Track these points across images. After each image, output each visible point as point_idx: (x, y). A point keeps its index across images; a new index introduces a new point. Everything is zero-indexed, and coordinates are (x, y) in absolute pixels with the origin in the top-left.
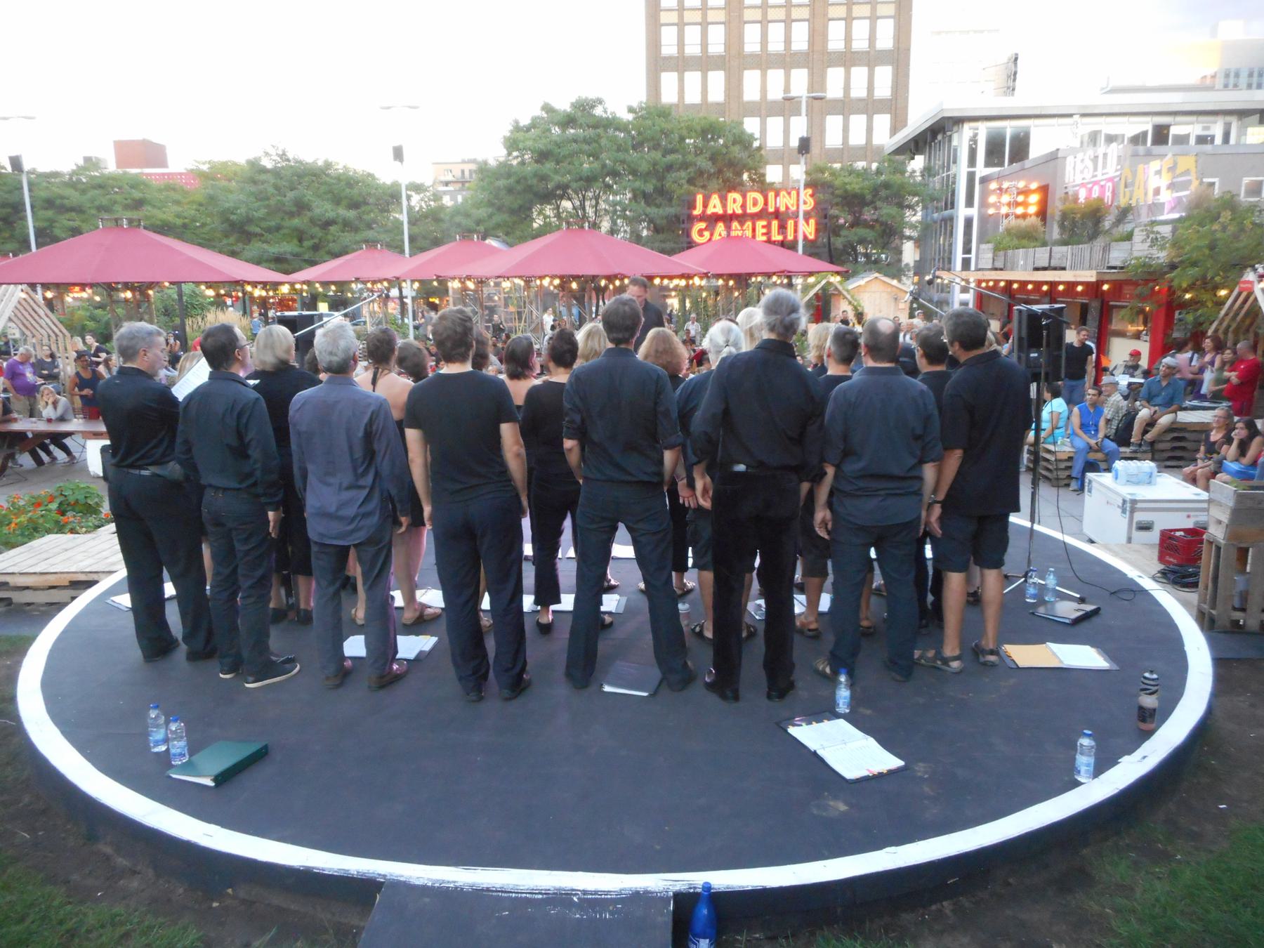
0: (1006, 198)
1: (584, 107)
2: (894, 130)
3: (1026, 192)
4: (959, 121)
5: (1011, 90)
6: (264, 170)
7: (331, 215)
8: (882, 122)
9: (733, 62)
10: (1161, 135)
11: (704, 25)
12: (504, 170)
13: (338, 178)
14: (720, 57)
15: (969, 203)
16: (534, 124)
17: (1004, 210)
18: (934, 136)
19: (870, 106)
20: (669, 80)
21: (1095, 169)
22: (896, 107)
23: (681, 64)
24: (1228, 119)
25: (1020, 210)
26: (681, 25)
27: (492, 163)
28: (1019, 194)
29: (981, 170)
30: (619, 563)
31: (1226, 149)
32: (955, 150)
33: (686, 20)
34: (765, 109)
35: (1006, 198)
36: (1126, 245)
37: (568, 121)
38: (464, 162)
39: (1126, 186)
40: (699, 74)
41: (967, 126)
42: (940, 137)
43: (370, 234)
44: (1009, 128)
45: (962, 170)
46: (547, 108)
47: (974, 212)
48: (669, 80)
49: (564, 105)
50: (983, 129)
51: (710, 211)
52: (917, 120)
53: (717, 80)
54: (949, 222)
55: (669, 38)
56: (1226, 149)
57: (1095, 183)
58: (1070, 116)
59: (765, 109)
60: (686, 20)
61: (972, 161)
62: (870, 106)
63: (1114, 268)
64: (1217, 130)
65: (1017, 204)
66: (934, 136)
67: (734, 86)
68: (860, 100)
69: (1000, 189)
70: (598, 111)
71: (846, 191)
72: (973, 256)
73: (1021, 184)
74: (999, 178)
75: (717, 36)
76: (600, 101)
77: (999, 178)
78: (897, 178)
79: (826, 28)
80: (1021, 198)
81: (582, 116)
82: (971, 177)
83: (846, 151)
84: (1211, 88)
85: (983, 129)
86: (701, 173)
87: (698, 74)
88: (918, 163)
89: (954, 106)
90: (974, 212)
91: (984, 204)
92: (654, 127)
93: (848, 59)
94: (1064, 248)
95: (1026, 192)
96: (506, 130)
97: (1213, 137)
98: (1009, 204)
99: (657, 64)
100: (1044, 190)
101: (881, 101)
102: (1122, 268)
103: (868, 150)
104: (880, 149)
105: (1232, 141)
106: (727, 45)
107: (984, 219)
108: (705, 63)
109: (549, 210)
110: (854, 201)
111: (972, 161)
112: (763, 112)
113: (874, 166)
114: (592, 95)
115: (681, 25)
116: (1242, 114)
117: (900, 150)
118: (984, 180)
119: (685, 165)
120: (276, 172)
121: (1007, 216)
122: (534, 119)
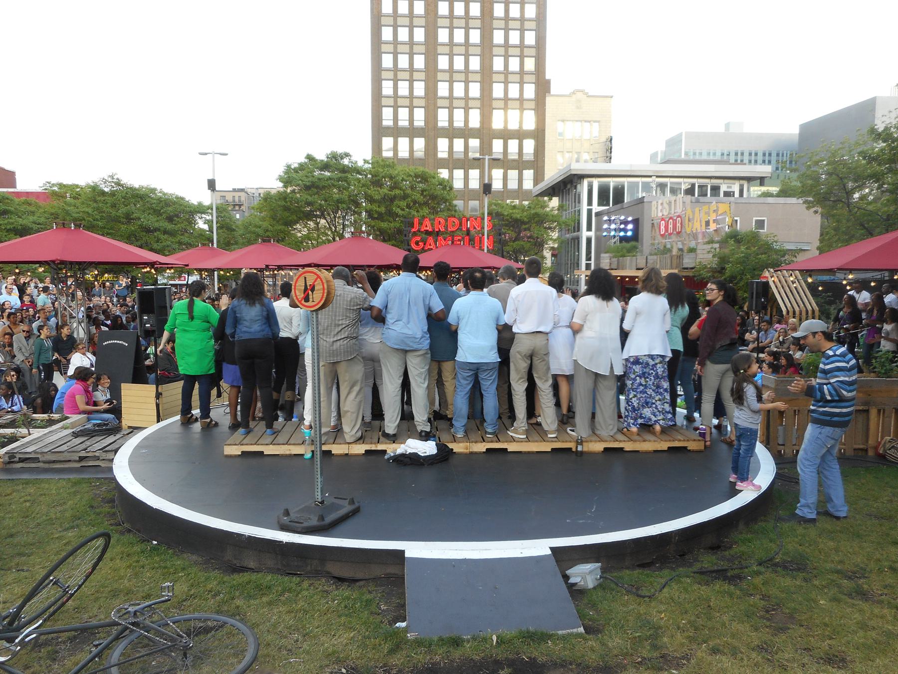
0: (613, 226)
1: (334, 156)
2: (536, 181)
3: (626, 223)
4: (581, 177)
5: (609, 159)
6: (103, 193)
7: (156, 225)
8: (528, 174)
9: (431, 132)
10: (715, 189)
11: (411, 108)
12: (282, 196)
13: (160, 200)
14: (422, 129)
15: (589, 229)
16: (302, 167)
17: (613, 233)
18: (565, 186)
19: (520, 164)
20: (387, 142)
21: (670, 209)
22: (537, 164)
23: (396, 132)
24: (742, 182)
25: (622, 234)
26: (396, 108)
27: (273, 192)
28: (621, 224)
29: (596, 208)
30: (512, 455)
31: (741, 200)
32: (579, 195)
33: (399, 104)
34: (452, 163)
35: (613, 226)
36: (692, 255)
37: (325, 166)
38: (234, 190)
39: (689, 221)
40: (392, 139)
41: (586, 182)
42: (569, 186)
43: (185, 239)
44: (612, 182)
45: (585, 207)
46: (310, 158)
47: (592, 234)
48: (387, 142)
49: (321, 156)
50: (596, 183)
51: (423, 229)
52: (553, 172)
53: (420, 143)
54: (577, 240)
55: (387, 114)
56: (741, 200)
57: (671, 218)
58: (650, 176)
59: (452, 163)
60: (399, 104)
61: (590, 203)
62: (520, 164)
63: (687, 269)
64: (736, 188)
65: (621, 230)
66: (567, 185)
67: (431, 148)
68: (514, 160)
69: (610, 220)
70: (346, 161)
71: (511, 217)
72: (592, 262)
73: (622, 218)
74: (608, 213)
75: (420, 116)
76: (347, 155)
77: (608, 213)
78: (540, 211)
79: (491, 114)
80: (622, 226)
81: (334, 163)
82: (590, 212)
83: (506, 192)
84: (727, 162)
85: (596, 183)
86: (415, 202)
87: (407, 140)
88: (555, 202)
89: (578, 168)
90: (592, 234)
91: (599, 229)
92: (381, 172)
93: (451, 133)
94: (655, 257)
95: (626, 223)
96: (280, 170)
97: (734, 192)
98: (615, 230)
99: (379, 131)
100: (636, 222)
101: (527, 161)
102: (692, 268)
103: (520, 192)
104: (529, 192)
105: (745, 195)
106: (426, 121)
107: (598, 239)
108: (412, 132)
109: (311, 224)
110: (516, 224)
111: (590, 203)
112: (451, 166)
113: (526, 203)
114: (340, 150)
115: (396, 108)
116: (749, 179)
117: (543, 194)
118: (597, 214)
119: (405, 197)
120: (113, 194)
121: (614, 237)
122: (301, 165)
